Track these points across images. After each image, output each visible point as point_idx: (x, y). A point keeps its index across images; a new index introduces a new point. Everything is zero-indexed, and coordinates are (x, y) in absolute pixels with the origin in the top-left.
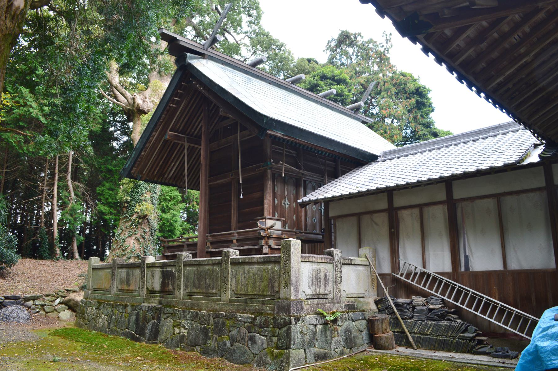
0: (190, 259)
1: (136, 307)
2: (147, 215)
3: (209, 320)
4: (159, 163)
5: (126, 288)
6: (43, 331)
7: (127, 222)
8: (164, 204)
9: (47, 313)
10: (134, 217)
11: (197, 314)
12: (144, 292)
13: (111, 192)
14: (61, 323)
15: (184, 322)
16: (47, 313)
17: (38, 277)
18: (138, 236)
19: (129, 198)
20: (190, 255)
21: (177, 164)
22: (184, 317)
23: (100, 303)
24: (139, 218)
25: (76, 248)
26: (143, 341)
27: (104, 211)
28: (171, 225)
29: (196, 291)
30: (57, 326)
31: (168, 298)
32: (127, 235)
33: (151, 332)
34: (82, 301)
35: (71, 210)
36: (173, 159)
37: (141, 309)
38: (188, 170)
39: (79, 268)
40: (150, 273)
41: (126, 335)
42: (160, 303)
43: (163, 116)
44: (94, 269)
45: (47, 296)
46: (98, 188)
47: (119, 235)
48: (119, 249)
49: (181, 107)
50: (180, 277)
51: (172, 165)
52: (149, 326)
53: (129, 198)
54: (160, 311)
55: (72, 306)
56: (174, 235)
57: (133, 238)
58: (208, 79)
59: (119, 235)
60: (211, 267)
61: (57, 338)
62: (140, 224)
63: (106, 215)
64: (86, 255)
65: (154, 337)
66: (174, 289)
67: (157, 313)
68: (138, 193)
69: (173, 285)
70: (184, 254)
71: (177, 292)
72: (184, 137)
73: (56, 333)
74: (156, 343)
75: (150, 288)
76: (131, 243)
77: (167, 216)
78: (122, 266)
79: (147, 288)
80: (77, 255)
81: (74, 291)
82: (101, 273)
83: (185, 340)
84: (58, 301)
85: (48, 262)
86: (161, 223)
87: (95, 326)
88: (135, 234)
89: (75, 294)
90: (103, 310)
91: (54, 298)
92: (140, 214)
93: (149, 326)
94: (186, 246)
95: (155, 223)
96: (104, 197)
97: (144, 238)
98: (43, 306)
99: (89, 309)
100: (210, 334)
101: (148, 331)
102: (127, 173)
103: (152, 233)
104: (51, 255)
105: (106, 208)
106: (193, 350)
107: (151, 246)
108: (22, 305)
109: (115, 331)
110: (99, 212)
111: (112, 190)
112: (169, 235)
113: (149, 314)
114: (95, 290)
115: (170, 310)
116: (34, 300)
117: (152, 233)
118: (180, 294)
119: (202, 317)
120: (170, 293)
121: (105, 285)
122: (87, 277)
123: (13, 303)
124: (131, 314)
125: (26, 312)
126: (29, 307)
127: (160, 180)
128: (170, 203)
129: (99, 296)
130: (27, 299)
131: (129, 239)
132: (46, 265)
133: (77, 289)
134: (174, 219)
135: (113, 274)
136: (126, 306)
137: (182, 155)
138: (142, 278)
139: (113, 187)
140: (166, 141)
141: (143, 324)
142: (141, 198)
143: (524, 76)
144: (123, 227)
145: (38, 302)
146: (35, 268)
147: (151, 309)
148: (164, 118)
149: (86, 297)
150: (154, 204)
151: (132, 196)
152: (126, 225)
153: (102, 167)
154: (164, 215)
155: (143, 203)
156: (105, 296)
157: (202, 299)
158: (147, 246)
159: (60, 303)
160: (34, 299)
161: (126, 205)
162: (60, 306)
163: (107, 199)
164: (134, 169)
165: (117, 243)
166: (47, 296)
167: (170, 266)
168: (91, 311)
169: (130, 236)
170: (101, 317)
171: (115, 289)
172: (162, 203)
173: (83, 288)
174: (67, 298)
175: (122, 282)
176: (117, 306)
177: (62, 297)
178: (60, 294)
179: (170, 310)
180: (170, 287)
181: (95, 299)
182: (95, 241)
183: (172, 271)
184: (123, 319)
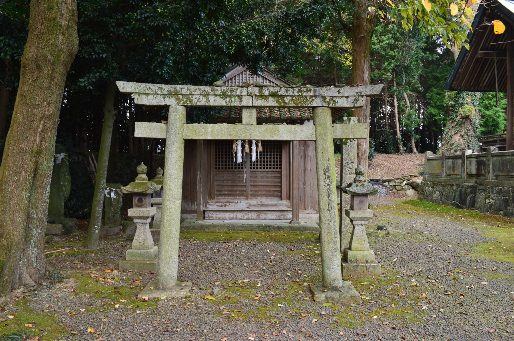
0: (497, 151)
1: (460, 185)
2: (469, 116)
3: (509, 193)
4: (474, 75)
5: (452, 172)
6: (398, 201)
7: (452, 122)
8: (486, 102)
9: (398, 191)
10: (458, 118)
11: (501, 189)
12: (465, 175)
13: (438, 96)
14: (408, 198)
15: (492, 195)
16: (398, 191)
17: (389, 167)
18: (463, 133)
19: (453, 103)
20: (497, 149)
21: (490, 74)
22: (492, 192)
23: (434, 184)
24: (463, 118)
25: (414, 145)
26: (465, 208)
27: (434, 113)
28: (494, 120)
29: (500, 174)
30: (405, 199)
31: (482, 179)
32: (453, 133)
33: (470, 202)
34: (422, 183)
35: (408, 116)
36: (487, 70)
37: (463, 187)
38: (498, 81)
39: (417, 159)
40: (468, 162)
41: (453, 205)
42: (476, 182)
43: (474, 39)
44: (429, 160)
45: (397, 179)
46: (428, 94)
47: (447, 133)
48: (447, 144)
49: (488, 31)
50: (489, 165)
51: (485, 76)
52: (469, 199)
53: (453, 103)
54: (476, 188)
55: (414, 187)
56: (498, 128)
57: (459, 135)
58: (507, 9)
59: (447, 133)
60: (510, 157)
61: (407, 205)
62: (464, 123)
63: (436, 116)
64: (422, 150)
65: (472, 206)
66: (486, 173)
67: (474, 190)
68: (460, 97)
69: (485, 170)
70: (492, 148)
71: (487, 175)
72: (493, 53)
73: (405, 202)
74: (473, 210)
75: (469, 173)
76: (457, 139)
77: (490, 113)
78: (449, 158)
79: (467, 173)
80: (415, 150)
81: (415, 176)
82: (434, 162)
83: (493, 207)
84: (404, 183)
85: (394, 156)
86: (484, 120)
87: (432, 199)
88: (460, 132)
89: (416, 178)
90: (437, 188)
91: (402, 181)
92: (463, 115)
93: (469, 199)
94: (498, 141)
95: (477, 120)
96: (433, 101)
97: (467, 135)
98: (395, 186)
99: (427, 188)
100: (510, 203)
101: (468, 202)
102: (448, 87)
103: (474, 130)
104: (397, 151)
105: (435, 110)
106: (498, 214)
107: (474, 141)
108: (381, 185)
109: (446, 202)
110: (429, 114)
111: (440, 94)
112: (493, 129)
113: (468, 190)
114: (430, 175)
115: (483, 187)
116: (389, 182)
117: (474, 130)
118: (490, 176)
119: (505, 192)
120: (482, 175)
121: (437, 171)
122: (424, 166)
123: (376, 184)
124: (456, 191)
125: (384, 190)
126: (386, 187)
127: (476, 89)
128: (493, 100)
129: (433, 179)
130: (384, 181)
131: (455, 136)
132: (394, 157)
133: (417, 174)
134: (496, 115)
135: (443, 163)
136: (452, 185)
137: (493, 68)
138: (463, 165)
139: (440, 92)
140: (478, 59)
141: (465, 197)
142: (463, 101)
143: (147, 299)
144: (450, 127)
145: (391, 183)
146: (387, 160)
147: (470, 187)
148: (475, 41)
149: (424, 180)
150: (475, 106)
151: (455, 101)
152: (452, 125)
153: (430, 75)
154: (487, 112)
155: (466, 106)
156: (438, 179)
157: (505, 180)
158: (470, 141)
159: (406, 184)
160: (389, 181)
161: (451, 108)
162: (406, 186)
163: (436, 102)
164: (454, 83)
165: (445, 140)
166: (397, 179)
167: (483, 157)
168: (429, 189)
169: (455, 134)
170: (435, 193)
171: (444, 174)
172: (484, 102)
173: (421, 174)
174: (411, 181)
175: (449, 169)
176: (446, 185)
177: (407, 180)
178: (406, 178)
179: (483, 187)
180: (483, 172)
181: (430, 181)
182: (428, 138)
183: (483, 160)
184: (451, 194)
